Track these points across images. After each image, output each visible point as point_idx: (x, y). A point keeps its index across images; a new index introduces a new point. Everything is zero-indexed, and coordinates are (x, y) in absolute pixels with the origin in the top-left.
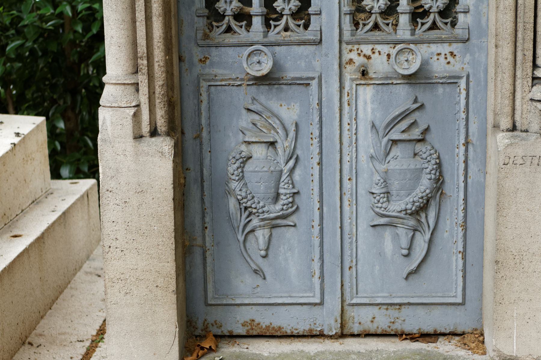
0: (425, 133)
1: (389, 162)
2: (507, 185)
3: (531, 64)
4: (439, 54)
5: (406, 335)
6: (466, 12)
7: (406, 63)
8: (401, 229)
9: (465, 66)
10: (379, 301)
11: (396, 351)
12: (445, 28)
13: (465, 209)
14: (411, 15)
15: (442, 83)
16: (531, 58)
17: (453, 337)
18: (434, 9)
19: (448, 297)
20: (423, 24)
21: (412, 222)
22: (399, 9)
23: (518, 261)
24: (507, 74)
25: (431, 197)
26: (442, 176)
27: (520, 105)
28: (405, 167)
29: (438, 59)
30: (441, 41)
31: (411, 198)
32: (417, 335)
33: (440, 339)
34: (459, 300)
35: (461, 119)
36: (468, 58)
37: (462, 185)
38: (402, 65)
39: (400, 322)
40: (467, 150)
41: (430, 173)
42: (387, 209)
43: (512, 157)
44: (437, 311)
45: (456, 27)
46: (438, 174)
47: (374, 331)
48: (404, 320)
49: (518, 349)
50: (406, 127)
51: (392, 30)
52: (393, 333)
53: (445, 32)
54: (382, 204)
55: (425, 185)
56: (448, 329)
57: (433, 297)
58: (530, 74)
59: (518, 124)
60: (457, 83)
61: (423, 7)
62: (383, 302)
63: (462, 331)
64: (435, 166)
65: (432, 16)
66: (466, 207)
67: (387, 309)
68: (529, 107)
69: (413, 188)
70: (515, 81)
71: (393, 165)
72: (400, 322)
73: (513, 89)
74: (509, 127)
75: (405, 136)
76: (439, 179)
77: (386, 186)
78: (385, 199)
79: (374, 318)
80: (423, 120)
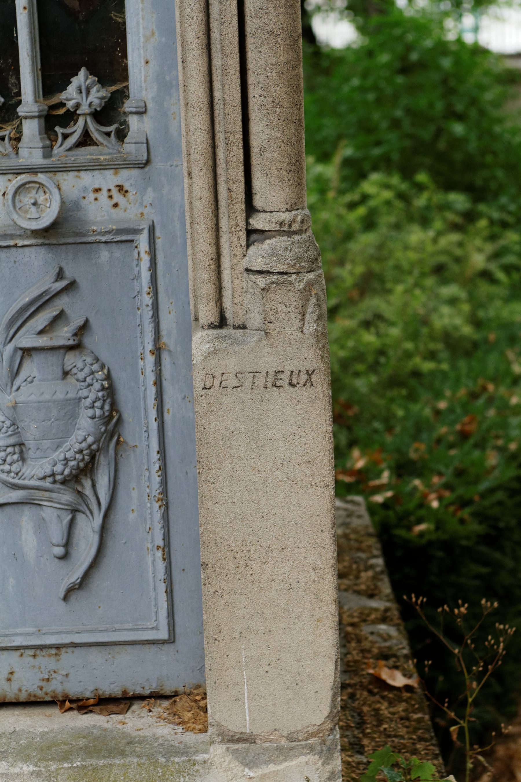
0: (82, 335)
1: (18, 389)
2: (213, 425)
3: (243, 206)
4: (97, 190)
5: (71, 701)
6: (142, 112)
7: (33, 209)
8: (48, 510)
9: (146, 211)
10: (18, 641)
11: (47, 733)
12: (105, 143)
13: (163, 469)
14: (43, 121)
15: (106, 242)
16: (242, 196)
17: (158, 702)
18: (84, 109)
19: (143, 629)
20: (65, 137)
21: (67, 497)
22: (21, 111)
23: (242, 562)
24: (203, 226)
25: (98, 450)
26: (117, 411)
27: (230, 281)
28: (47, 397)
29: (96, 199)
30: (101, 167)
31: (61, 452)
32: (92, 701)
33: (135, 707)
34: (163, 634)
35: (144, 307)
36: (150, 195)
37: (154, 426)
38: (26, 212)
39: (59, 678)
40: (158, 362)
41: (93, 407)
42: (20, 474)
43: (218, 375)
44: (125, 657)
45: (126, 140)
46: (107, 407)
47: (13, 696)
48: (67, 675)
49: (253, 721)
50: (45, 324)
51: (10, 149)
52: (48, 698)
53: (106, 150)
54: (10, 464)
55: (85, 428)
56: (147, 688)
57: (115, 630)
58: (242, 224)
59: (228, 315)
60: (132, 241)
61: (64, 105)
62: (25, 643)
63: (174, 690)
64: (100, 394)
65: (81, 122)
66: (165, 465)
67: (34, 656)
68: (244, 284)
69: (66, 435)
70: (217, 238)
71: (27, 394)
72: (59, 678)
73: (214, 251)
74: (212, 320)
75: (43, 341)
76: (111, 417)
77: (16, 433)
78: (16, 457)
79: (12, 673)
80: (76, 309)
